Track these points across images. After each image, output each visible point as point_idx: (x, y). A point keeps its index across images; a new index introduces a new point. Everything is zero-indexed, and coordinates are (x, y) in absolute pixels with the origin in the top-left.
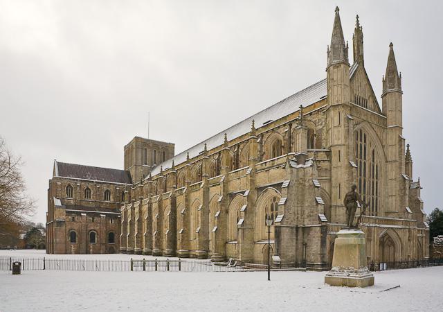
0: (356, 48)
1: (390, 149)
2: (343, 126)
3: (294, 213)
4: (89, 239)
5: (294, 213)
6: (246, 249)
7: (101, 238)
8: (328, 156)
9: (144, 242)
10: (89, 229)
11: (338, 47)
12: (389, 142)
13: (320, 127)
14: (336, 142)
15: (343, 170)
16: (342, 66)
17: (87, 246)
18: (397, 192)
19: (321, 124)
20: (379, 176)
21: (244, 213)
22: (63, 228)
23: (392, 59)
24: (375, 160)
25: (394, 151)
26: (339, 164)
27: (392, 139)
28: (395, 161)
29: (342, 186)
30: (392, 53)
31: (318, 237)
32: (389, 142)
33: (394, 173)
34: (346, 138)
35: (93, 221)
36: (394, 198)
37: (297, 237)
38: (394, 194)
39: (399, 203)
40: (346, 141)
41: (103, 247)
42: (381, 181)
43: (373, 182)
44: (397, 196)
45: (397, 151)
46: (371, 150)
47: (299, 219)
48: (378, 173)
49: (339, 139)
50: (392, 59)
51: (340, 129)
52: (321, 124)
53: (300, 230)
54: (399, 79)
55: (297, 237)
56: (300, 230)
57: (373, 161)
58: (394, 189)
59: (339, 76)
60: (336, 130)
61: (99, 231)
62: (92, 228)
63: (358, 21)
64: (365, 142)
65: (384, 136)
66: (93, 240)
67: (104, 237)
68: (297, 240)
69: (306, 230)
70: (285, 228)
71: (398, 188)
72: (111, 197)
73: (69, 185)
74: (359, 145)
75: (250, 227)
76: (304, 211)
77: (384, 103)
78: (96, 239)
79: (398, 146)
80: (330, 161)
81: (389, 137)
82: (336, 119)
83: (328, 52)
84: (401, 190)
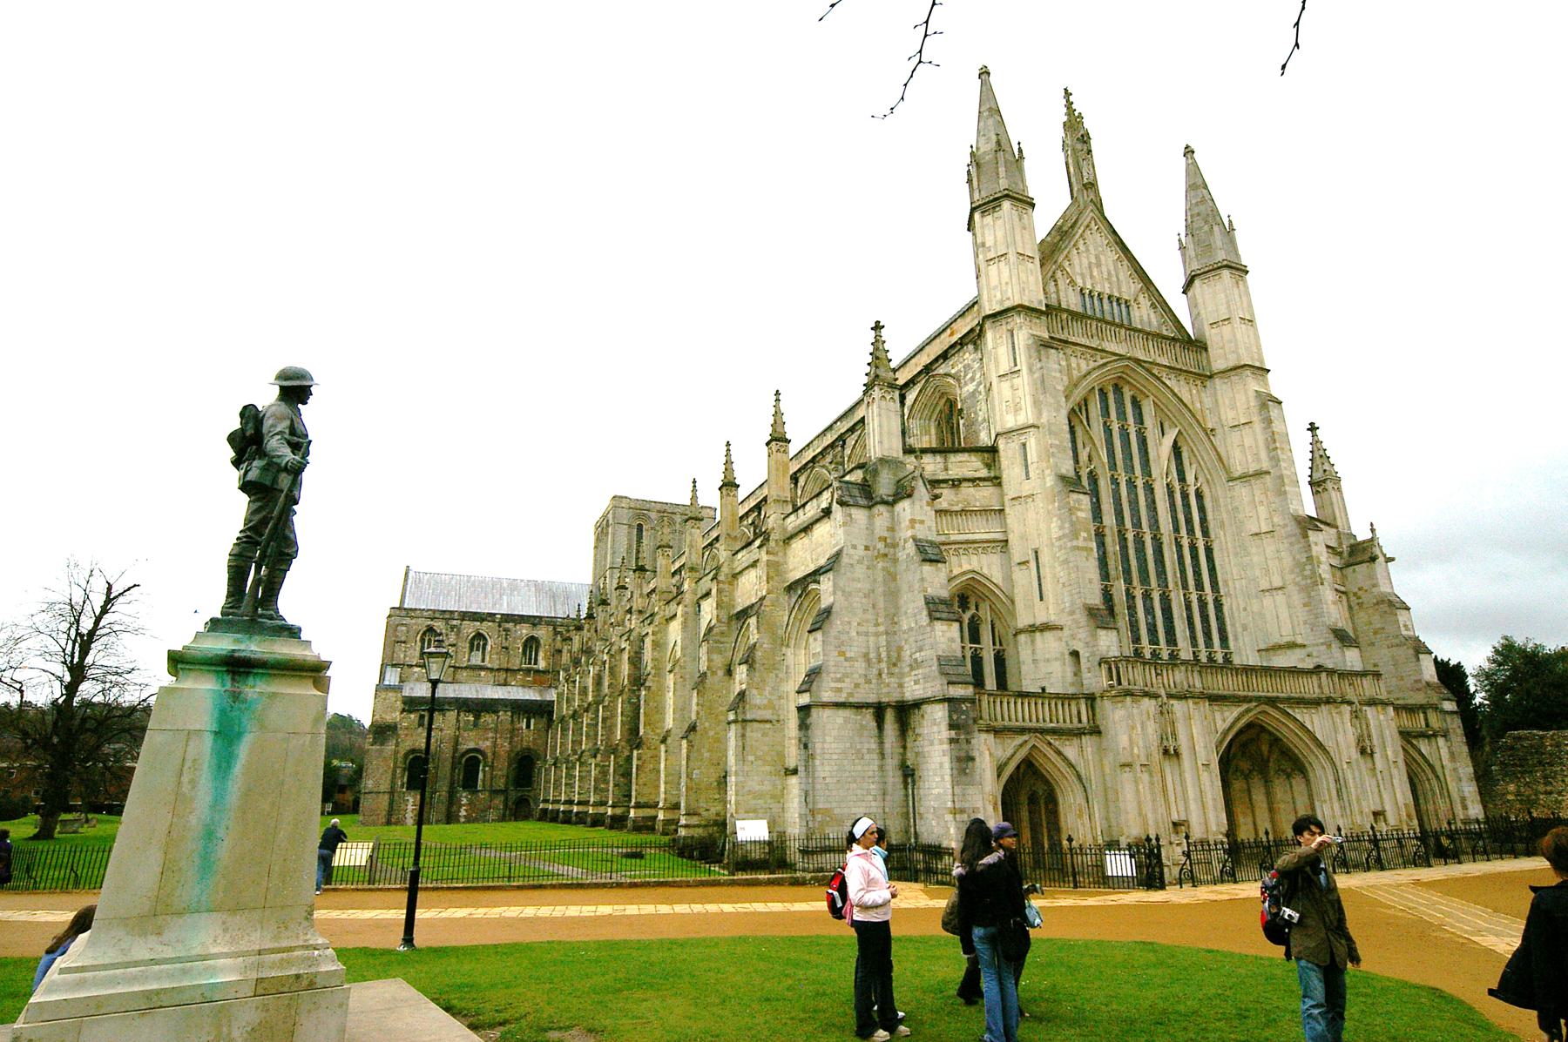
0: (1072, 169)
1: (1235, 436)
2: (1025, 371)
3: (866, 656)
8: (988, 466)
9: (662, 776)
10: (463, 748)
11: (972, 154)
13: (971, 387)
14: (1010, 422)
16: (1006, 204)
17: (452, 799)
18: (1289, 577)
19: (972, 379)
21: (744, 668)
22: (390, 747)
23: (1196, 185)
24: (1190, 478)
25: (1248, 441)
26: (1027, 488)
27: (1234, 407)
28: (1259, 474)
29: (1045, 558)
30: (987, 94)
32: (1229, 416)
33: (1262, 510)
34: (1036, 403)
37: (881, 743)
38: (1277, 582)
39: (1302, 614)
40: (1040, 414)
41: (498, 801)
44: (1291, 588)
45: (1261, 444)
46: (1168, 441)
47: (884, 676)
48: (1210, 516)
49: (1017, 409)
50: (1196, 185)
51: (1017, 381)
52: (972, 379)
53: (890, 716)
55: (881, 743)
56: (890, 716)
57: (1182, 479)
59: (1000, 234)
60: (1005, 385)
61: (489, 755)
64: (1140, 419)
65: (1208, 401)
66: (470, 782)
67: (502, 768)
68: (882, 755)
69: (906, 712)
70: (828, 712)
71: (1288, 561)
73: (430, 629)
74: (1198, 533)
76: (900, 649)
77: (1193, 305)
78: (481, 775)
79: (1258, 426)
80: (996, 481)
82: (1003, 352)
83: (1182, 248)
84: (1299, 566)
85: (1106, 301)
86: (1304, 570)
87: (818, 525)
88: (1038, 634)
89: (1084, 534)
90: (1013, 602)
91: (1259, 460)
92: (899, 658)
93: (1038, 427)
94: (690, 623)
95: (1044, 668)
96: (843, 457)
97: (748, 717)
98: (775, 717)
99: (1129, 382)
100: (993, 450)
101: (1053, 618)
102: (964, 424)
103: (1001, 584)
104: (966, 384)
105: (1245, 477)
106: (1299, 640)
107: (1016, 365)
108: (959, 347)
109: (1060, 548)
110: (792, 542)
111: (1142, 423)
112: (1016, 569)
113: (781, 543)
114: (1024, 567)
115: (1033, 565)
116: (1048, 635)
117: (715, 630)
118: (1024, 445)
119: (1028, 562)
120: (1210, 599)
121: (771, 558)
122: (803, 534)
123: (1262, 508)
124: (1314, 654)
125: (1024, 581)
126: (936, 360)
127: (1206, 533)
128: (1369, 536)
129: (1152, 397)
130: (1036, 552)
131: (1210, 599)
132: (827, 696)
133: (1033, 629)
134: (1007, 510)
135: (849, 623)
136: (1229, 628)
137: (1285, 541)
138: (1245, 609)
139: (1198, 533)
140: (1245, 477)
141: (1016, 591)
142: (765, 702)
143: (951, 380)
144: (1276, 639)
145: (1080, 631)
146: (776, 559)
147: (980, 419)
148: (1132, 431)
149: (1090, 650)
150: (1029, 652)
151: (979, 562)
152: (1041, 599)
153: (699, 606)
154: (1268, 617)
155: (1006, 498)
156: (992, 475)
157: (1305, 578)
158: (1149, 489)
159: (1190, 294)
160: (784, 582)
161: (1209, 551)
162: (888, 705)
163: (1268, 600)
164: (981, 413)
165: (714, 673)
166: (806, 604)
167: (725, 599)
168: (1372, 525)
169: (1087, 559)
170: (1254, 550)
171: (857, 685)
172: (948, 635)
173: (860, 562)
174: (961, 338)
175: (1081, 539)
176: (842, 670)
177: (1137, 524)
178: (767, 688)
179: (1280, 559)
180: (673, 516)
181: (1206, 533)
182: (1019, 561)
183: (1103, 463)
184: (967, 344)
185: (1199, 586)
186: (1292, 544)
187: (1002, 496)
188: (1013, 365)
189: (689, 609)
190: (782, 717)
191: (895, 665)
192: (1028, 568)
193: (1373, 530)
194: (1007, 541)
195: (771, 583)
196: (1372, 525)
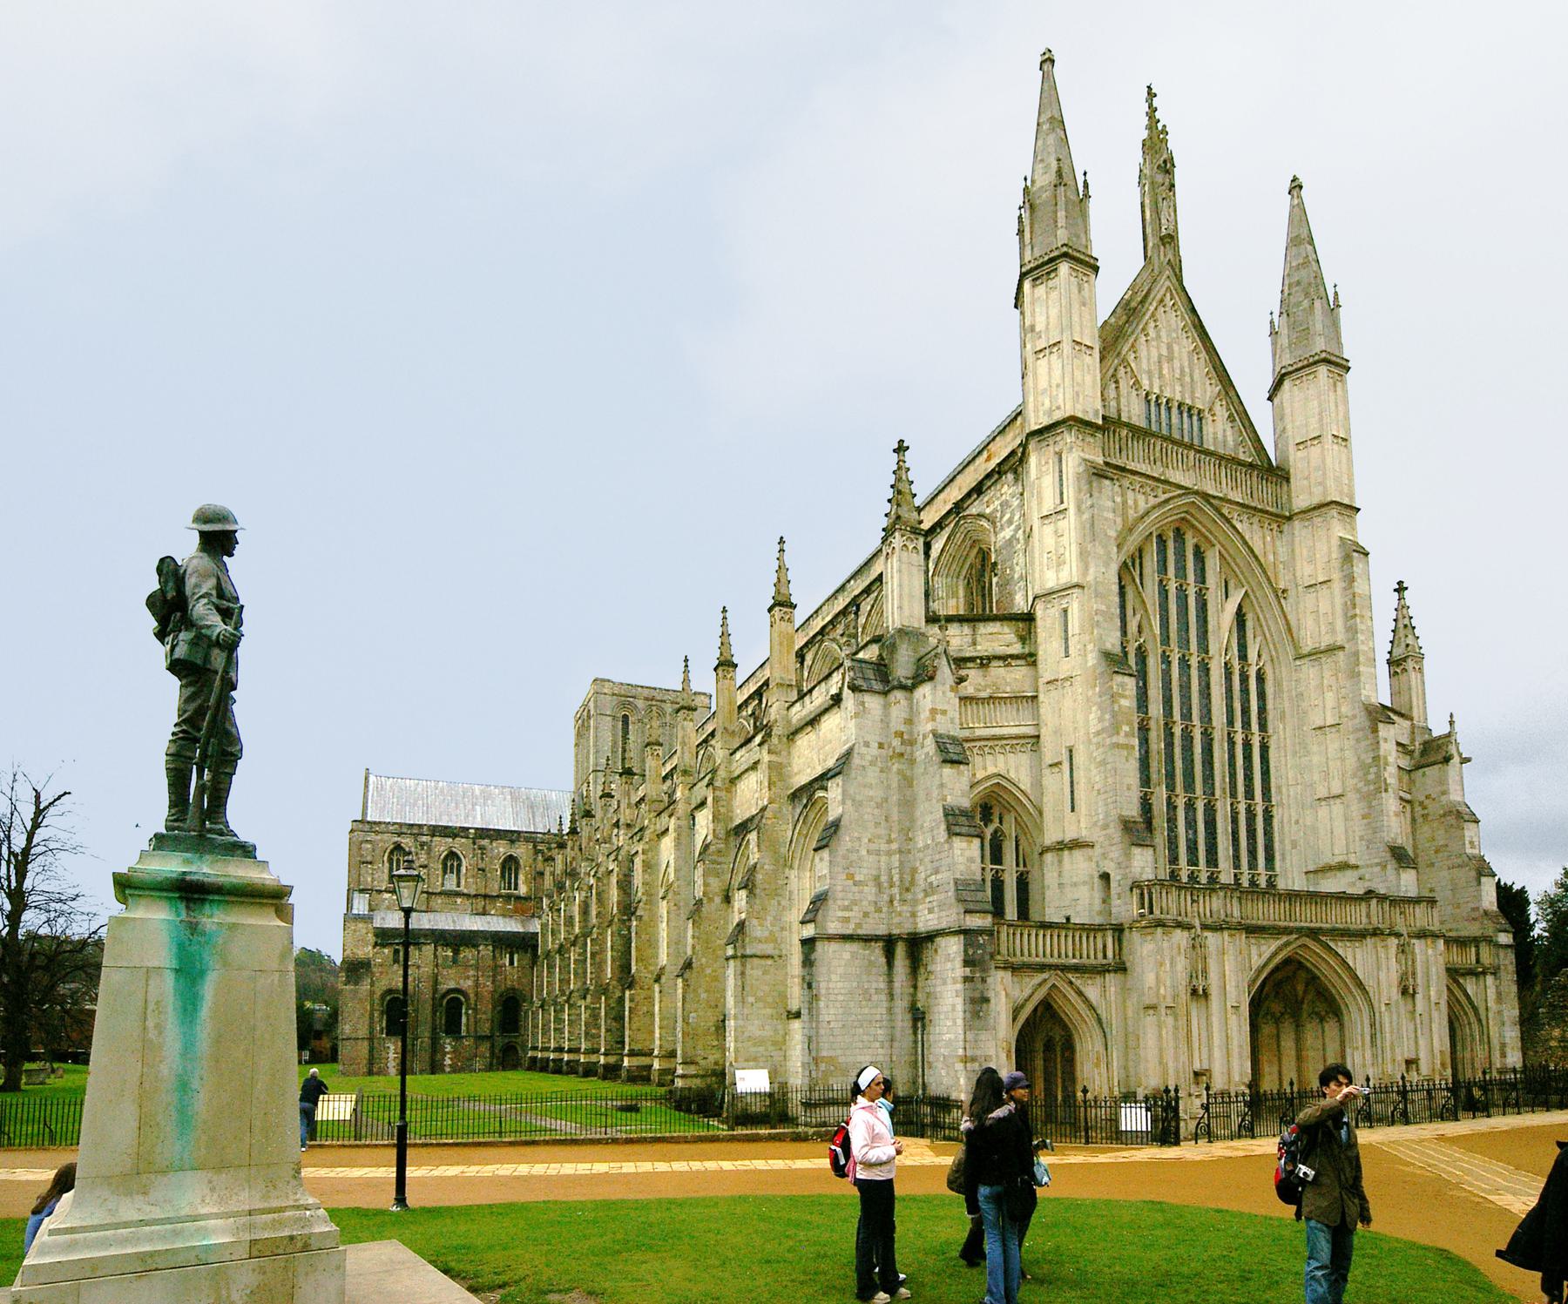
1: (1309, 600)
4: (442, 1020)
5: (877, 878)
6: (760, 1042)
7: (478, 1017)
8: (1023, 639)
10: (443, 987)
12: (1306, 572)
14: (1051, 580)
15: (1079, 687)
19: (1010, 522)
20: (1271, 716)
22: (365, 987)
23: (1300, 239)
24: (1252, 655)
25: (1324, 607)
26: (1066, 668)
27: (1312, 561)
28: (1333, 649)
31: (955, 981)
32: (1306, 572)
35: (455, 961)
36: (1337, 807)
37: (890, 982)
38: (1336, 790)
41: (484, 1048)
42: (1281, 735)
43: (1247, 745)
44: (1352, 796)
48: (1270, 706)
49: (1060, 563)
51: (1062, 524)
54: (1333, 309)
55: (890, 982)
56: (900, 950)
57: (1243, 657)
58: (1334, 766)
59: (1054, 312)
62: (452, 985)
63: (1152, 110)
64: (1201, 577)
65: (1282, 551)
66: (453, 1027)
69: (918, 945)
70: (833, 947)
72: (521, 877)
73: (398, 847)
74: (1255, 727)
75: (768, 949)
76: (914, 871)
77: (1278, 417)
79: (1337, 586)
80: (1030, 659)
81: (1302, 551)
84: (1363, 768)
85: (1175, 411)
86: (1368, 773)
87: (826, 717)
88: (1066, 853)
89: (1126, 728)
90: (1041, 813)
91: (1333, 631)
92: (913, 882)
93: (1083, 587)
94: (684, 840)
95: (1070, 894)
96: (856, 627)
97: (748, 952)
98: (777, 952)
99: (1193, 526)
100: (1029, 618)
101: (1085, 834)
102: (997, 583)
103: (1029, 791)
104: (1002, 528)
105: (1315, 654)
106: (1353, 861)
107: (1062, 502)
108: (996, 476)
109: (1098, 745)
110: (797, 737)
111: (1204, 582)
112: (1046, 772)
113: (785, 739)
114: (1056, 770)
115: (1066, 766)
116: (1077, 853)
117: (712, 848)
118: (1065, 611)
119: (1060, 763)
120: (1259, 810)
121: (774, 758)
122: (810, 728)
123: (1331, 694)
124: (1367, 877)
125: (1054, 784)
126: (969, 495)
127: (1263, 727)
128: (1446, 730)
129: (1218, 546)
130: (1071, 751)
131: (1259, 810)
132: (833, 927)
133: (1062, 847)
134: (1041, 697)
135: (859, 839)
136: (1277, 845)
137: (1351, 737)
138: (1297, 822)
139: (1255, 727)
140: (1315, 654)
141: (1045, 800)
142: (767, 933)
143: (984, 523)
144: (1328, 859)
145: (1113, 848)
146: (779, 760)
147: (1016, 576)
148: (1192, 592)
149: (1122, 871)
150: (1056, 874)
151: (1006, 763)
152: (1073, 810)
153: (694, 819)
154: (1322, 832)
155: (1042, 681)
156: (1027, 651)
157: (1368, 783)
158: (1205, 669)
159: (1276, 400)
160: (787, 789)
161: (1264, 748)
162: (899, 937)
163: (1323, 812)
164: (1017, 568)
165: (711, 900)
166: (812, 816)
167: (722, 810)
168: (1451, 716)
169: (1127, 760)
170: (1315, 748)
171: (866, 915)
172: (968, 854)
173: (872, 763)
174: (999, 465)
175: (1122, 734)
176: (850, 896)
177: (1187, 716)
178: (769, 918)
179: (1343, 760)
180: (663, 705)
181: (1263, 727)
182: (1050, 762)
183: (1154, 636)
184: (1006, 473)
185: (1249, 794)
186: (1358, 740)
187: (1036, 678)
188: (1058, 501)
189: (683, 823)
190: (784, 952)
191: (908, 890)
192: (1060, 771)
193: (1451, 723)
194: (1038, 737)
195: (773, 789)
196: (1451, 716)
